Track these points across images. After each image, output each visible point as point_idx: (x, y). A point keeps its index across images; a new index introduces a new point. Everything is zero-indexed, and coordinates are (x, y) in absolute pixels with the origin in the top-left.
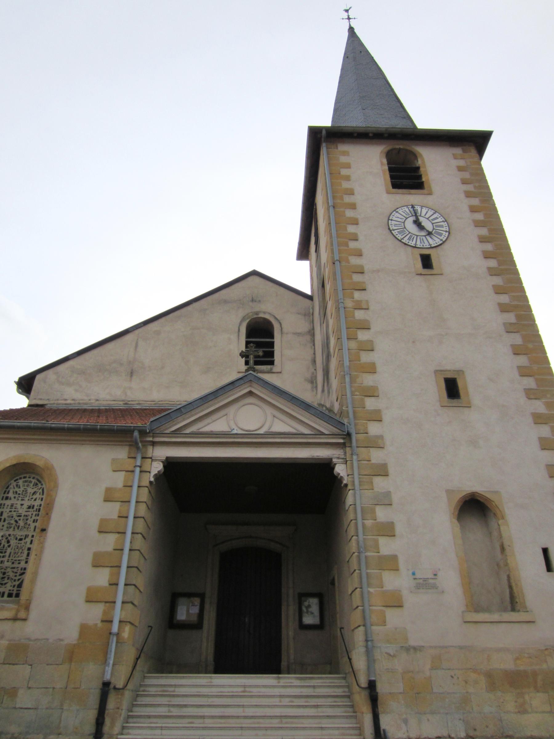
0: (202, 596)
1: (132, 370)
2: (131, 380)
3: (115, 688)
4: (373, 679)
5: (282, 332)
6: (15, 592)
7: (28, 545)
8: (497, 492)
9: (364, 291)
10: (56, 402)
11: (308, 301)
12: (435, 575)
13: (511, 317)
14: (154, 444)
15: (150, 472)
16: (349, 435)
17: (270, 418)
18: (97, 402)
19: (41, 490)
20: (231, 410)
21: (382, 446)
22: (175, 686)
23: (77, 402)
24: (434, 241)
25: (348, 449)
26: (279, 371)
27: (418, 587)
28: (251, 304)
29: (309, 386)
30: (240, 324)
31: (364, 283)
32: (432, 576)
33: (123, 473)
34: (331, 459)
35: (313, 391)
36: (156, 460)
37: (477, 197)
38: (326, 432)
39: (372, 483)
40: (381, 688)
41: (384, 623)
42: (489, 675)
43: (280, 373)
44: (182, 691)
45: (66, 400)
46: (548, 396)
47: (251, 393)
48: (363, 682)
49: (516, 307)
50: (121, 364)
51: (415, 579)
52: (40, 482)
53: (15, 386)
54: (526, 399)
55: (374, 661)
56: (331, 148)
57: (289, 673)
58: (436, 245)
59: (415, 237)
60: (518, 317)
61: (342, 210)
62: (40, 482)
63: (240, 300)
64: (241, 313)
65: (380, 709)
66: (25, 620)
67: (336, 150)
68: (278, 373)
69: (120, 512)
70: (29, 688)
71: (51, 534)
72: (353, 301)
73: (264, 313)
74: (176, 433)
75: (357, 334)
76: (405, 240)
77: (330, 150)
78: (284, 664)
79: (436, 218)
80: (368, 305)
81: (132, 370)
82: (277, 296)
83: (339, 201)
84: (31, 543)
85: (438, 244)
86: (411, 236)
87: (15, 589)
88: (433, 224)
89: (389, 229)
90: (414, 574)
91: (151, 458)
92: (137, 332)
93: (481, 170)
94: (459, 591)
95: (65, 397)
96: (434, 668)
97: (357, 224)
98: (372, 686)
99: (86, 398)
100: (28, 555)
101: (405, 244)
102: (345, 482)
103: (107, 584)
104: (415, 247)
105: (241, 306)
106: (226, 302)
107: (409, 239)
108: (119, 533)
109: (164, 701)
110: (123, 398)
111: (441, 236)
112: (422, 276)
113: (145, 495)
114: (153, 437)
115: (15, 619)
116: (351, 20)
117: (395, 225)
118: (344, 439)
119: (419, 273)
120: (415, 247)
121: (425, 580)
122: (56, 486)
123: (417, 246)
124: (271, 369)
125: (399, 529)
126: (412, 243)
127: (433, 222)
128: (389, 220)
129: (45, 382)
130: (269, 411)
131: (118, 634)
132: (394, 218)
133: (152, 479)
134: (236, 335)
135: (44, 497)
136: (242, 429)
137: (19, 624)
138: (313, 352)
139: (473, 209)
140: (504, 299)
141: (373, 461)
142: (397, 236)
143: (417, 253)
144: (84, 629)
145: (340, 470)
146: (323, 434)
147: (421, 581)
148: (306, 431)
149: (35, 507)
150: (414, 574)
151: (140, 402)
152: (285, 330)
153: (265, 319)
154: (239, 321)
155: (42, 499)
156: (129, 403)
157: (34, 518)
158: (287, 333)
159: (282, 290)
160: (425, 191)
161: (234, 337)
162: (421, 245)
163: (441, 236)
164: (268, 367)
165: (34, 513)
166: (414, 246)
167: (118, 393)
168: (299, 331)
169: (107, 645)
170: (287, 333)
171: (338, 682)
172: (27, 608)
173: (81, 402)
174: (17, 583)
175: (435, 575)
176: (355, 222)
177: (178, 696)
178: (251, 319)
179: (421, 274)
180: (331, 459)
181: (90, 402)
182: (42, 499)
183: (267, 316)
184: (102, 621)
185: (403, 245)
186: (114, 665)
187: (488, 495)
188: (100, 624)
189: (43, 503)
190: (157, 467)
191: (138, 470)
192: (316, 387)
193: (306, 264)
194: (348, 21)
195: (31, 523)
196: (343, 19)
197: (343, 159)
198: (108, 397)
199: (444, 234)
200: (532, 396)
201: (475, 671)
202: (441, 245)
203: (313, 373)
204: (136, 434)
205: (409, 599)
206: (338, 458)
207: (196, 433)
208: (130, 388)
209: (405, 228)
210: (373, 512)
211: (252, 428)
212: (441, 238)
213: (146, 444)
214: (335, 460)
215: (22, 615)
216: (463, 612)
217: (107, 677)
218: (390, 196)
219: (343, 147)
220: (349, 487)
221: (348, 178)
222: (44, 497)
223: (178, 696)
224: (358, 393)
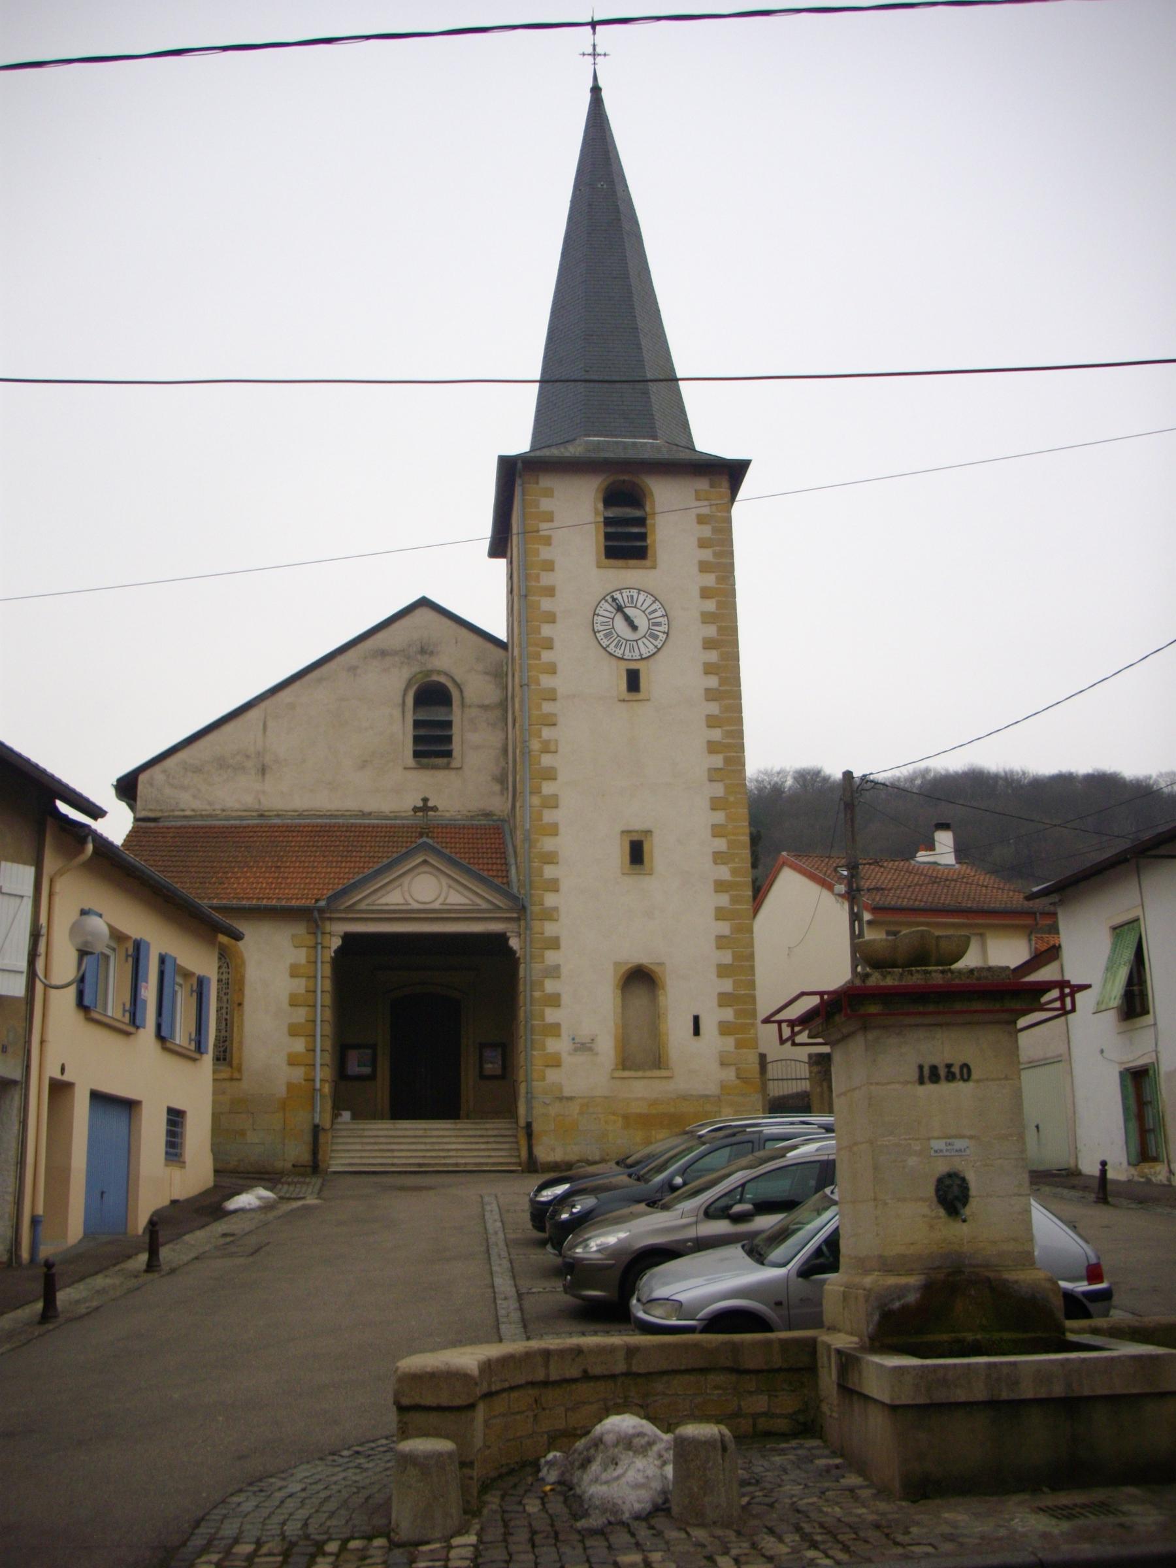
0: (374, 1047)
1: (263, 765)
2: (263, 781)
3: (323, 1129)
4: (530, 1120)
5: (463, 705)
6: (222, 1057)
7: (225, 1016)
8: (661, 964)
9: (552, 728)
10: (171, 814)
11: (499, 653)
12: (593, 1040)
13: (718, 761)
14: (330, 919)
15: (330, 948)
16: (524, 908)
17: (445, 889)
18: (224, 813)
19: (225, 964)
20: (406, 880)
21: (556, 918)
22: (363, 1129)
23: (198, 813)
24: (646, 648)
25: (522, 923)
26: (459, 766)
27: (576, 1050)
28: (419, 657)
29: (497, 788)
30: (405, 695)
31: (555, 715)
32: (590, 1041)
33: (305, 949)
34: (505, 933)
35: (502, 794)
36: (334, 935)
37: (713, 572)
38: (504, 907)
39: (543, 956)
40: (536, 1127)
41: (544, 1079)
42: (626, 1117)
43: (460, 768)
44: (367, 1133)
45: (183, 810)
46: (737, 860)
47: (425, 862)
48: (522, 1122)
49: (728, 747)
50: (248, 757)
51: (574, 1043)
52: (223, 956)
53: (113, 792)
54: (712, 863)
55: (532, 1108)
56: (529, 483)
57: (468, 1119)
58: (649, 654)
59: (625, 642)
60: (727, 761)
61: (538, 598)
62: (223, 956)
63: (404, 650)
64: (406, 673)
65: (534, 1142)
66: (240, 1080)
67: (535, 486)
68: (457, 769)
69: (306, 987)
70: (255, 1130)
71: (247, 1006)
72: (540, 742)
73: (439, 672)
74: (350, 909)
75: (541, 787)
76: (611, 649)
77: (528, 485)
78: (462, 1113)
79: (655, 611)
80: (557, 746)
81: (263, 765)
82: (456, 643)
83: (533, 583)
84: (227, 1014)
85: (652, 653)
86: (619, 641)
87: (222, 1053)
88: (649, 620)
89: (594, 630)
90: (573, 1039)
91: (330, 933)
92: (263, 705)
93: (728, 520)
94: (612, 1053)
95: (182, 806)
96: (581, 1113)
97: (554, 622)
98: (529, 1125)
99: (208, 807)
100: (226, 1024)
101: (610, 654)
102: (518, 955)
103: (304, 1050)
104: (622, 659)
105: (406, 661)
106: (383, 653)
107: (616, 646)
108: (309, 1006)
109: (357, 1140)
110: (257, 807)
111: (656, 639)
112: (626, 703)
113: (328, 970)
114: (330, 913)
115: (232, 1079)
116: (598, 59)
117: (602, 624)
118: (517, 913)
119: (621, 698)
120: (622, 659)
121: (583, 1044)
122: (243, 963)
123: (625, 657)
124: (449, 763)
125: (565, 999)
126: (619, 653)
127: (651, 617)
128: (594, 614)
129: (152, 785)
130: (445, 881)
131: (320, 1090)
132: (602, 612)
133: (333, 955)
134: (400, 709)
135: (230, 970)
136: (418, 902)
137: (235, 1083)
138: (504, 737)
139: (705, 593)
140: (716, 735)
141: (547, 934)
142: (601, 642)
143: (624, 666)
144: (290, 1086)
145: (514, 943)
146: (499, 908)
147: (579, 1045)
148: (484, 905)
149: (224, 982)
150: (573, 1039)
151: (281, 813)
152: (467, 701)
153: (439, 683)
154: (403, 686)
155: (229, 973)
156: (266, 813)
157: (224, 991)
158: (470, 706)
159: (464, 632)
160: (647, 563)
161: (397, 713)
162: (630, 655)
163: (656, 639)
164: (445, 760)
165: (224, 986)
166: (621, 656)
167: (249, 800)
168: (487, 702)
169: (313, 1098)
170: (470, 706)
171: (509, 1126)
172: (240, 1070)
173: (204, 813)
174: (222, 1049)
175: (593, 1040)
176: (551, 618)
177: (366, 1137)
178: (420, 686)
179: (624, 701)
180: (505, 933)
181: (214, 813)
182: (229, 973)
183: (442, 679)
184: (305, 1080)
185: (608, 655)
186: (320, 1112)
187: (651, 966)
188: (303, 1082)
189: (230, 976)
190: (336, 943)
191: (319, 946)
192: (507, 789)
193: (502, 563)
194: (591, 59)
195: (223, 995)
196: (584, 54)
197: (545, 504)
198: (237, 806)
199: (660, 638)
200: (719, 861)
201: (614, 1114)
202: (654, 654)
203: (503, 768)
204: (316, 914)
205: (567, 1059)
206: (513, 932)
207: (451, 1169)
208: (264, 792)
209: (613, 628)
210: (542, 984)
211: (427, 899)
212: (656, 643)
213: (324, 919)
214: (509, 934)
215: (236, 1075)
216: (613, 1070)
217: (317, 1121)
218: (602, 571)
219: (546, 482)
220: (522, 961)
221: (547, 541)
222: (230, 970)
223: (366, 1137)
224: (536, 860)
